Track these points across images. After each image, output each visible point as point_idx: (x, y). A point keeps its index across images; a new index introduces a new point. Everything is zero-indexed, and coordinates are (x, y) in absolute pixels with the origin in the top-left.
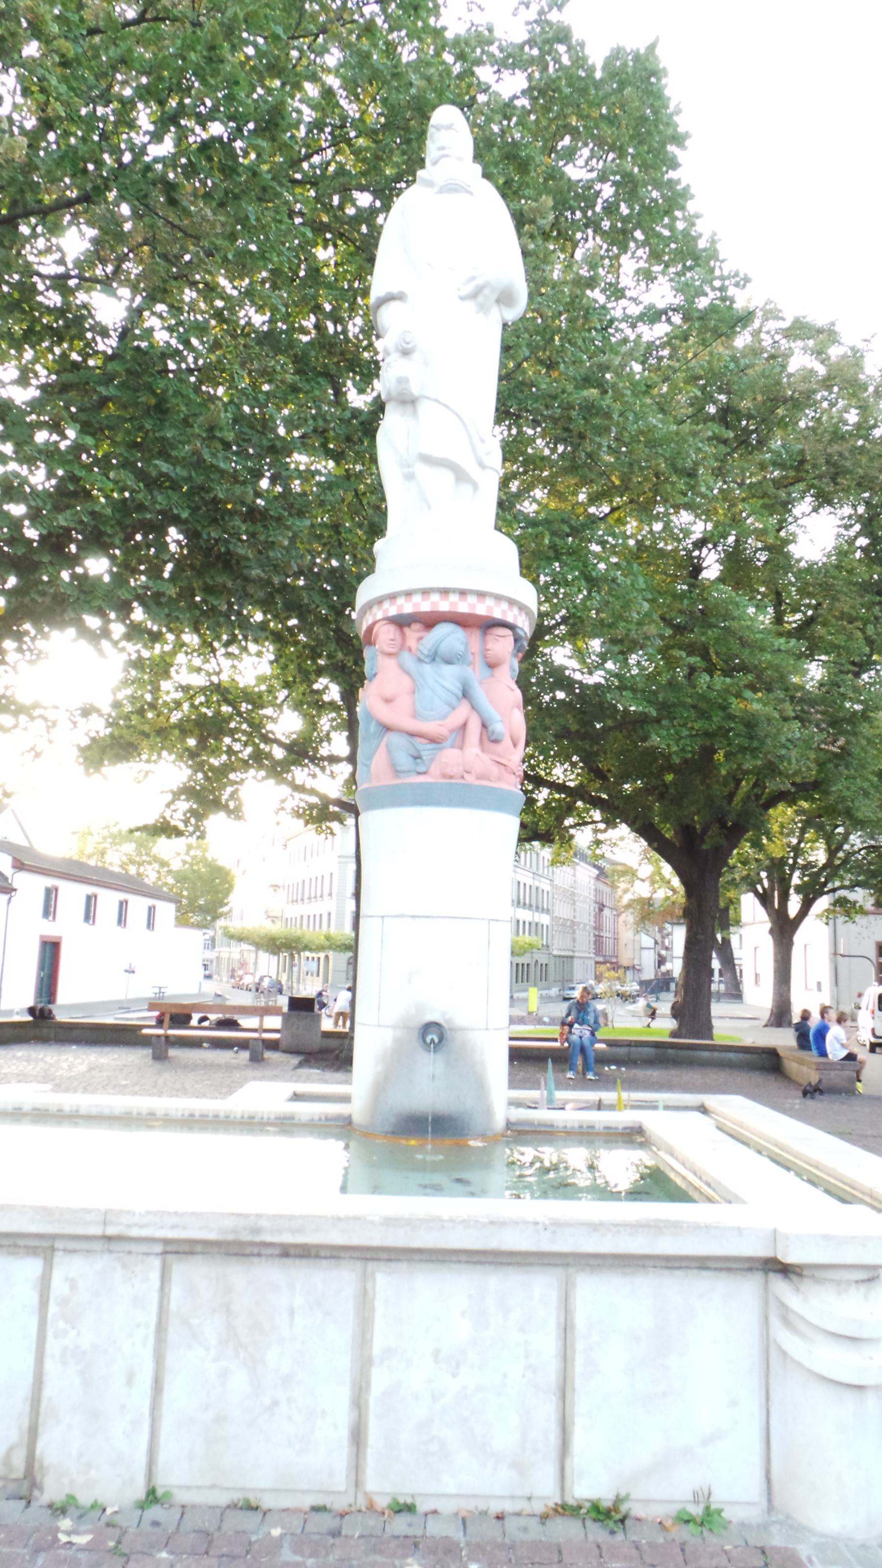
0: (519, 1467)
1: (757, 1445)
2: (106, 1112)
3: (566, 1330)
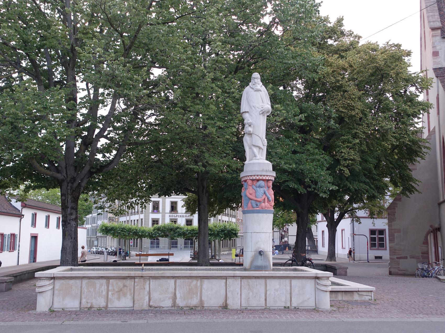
0: (286, 303)
1: (314, 300)
3: (291, 286)
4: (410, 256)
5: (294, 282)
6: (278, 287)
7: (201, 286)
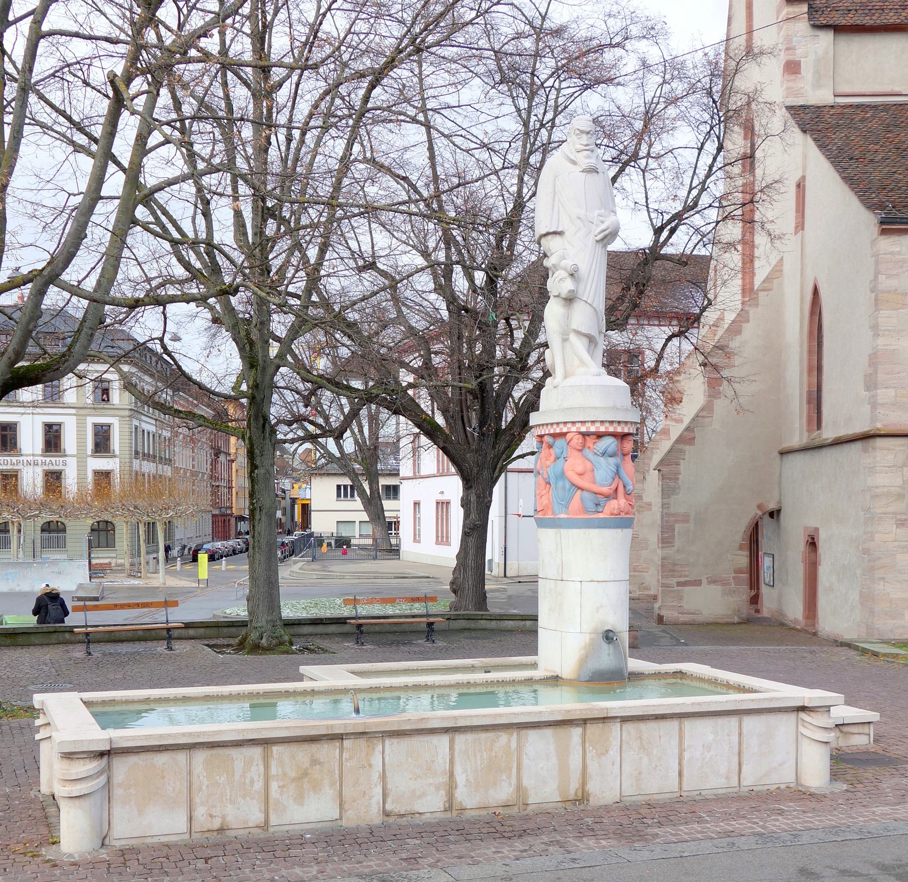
0: (727, 778)
2: (448, 683)
3: (740, 734)
4: (707, 578)
5: (749, 722)
6: (711, 737)
7: (519, 748)
